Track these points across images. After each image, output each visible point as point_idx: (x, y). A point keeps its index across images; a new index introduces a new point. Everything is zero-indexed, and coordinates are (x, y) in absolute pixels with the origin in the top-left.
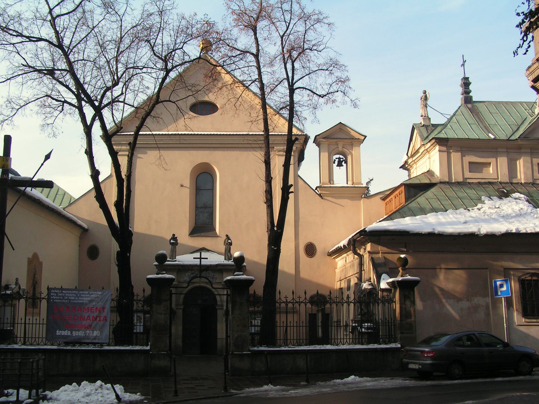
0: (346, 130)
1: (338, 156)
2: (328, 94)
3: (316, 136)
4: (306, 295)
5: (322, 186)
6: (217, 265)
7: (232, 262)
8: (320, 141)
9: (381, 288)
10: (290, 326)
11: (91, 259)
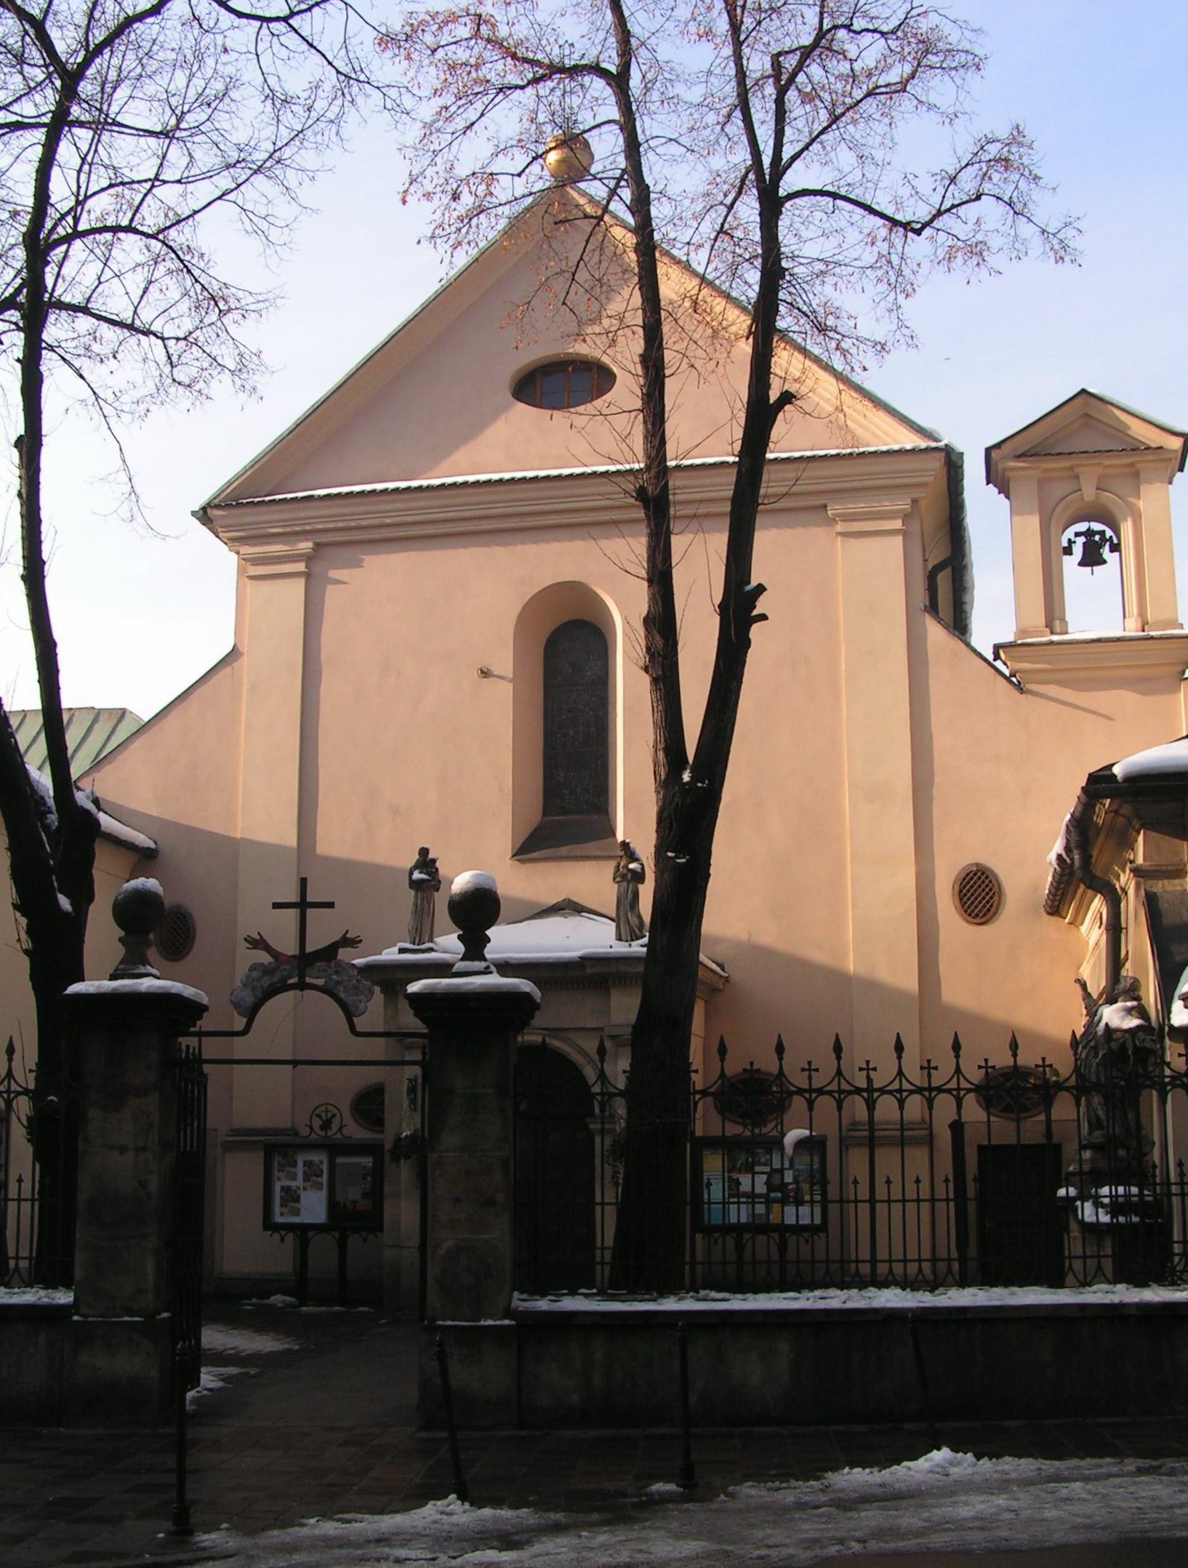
0: (1104, 419)
1: (1082, 527)
2: (939, 213)
3: (988, 451)
4: (957, 1056)
5: (1019, 642)
6: (583, 959)
7: (642, 946)
8: (1004, 470)
9: (1171, 1027)
10: (889, 1201)
11: (168, 959)
